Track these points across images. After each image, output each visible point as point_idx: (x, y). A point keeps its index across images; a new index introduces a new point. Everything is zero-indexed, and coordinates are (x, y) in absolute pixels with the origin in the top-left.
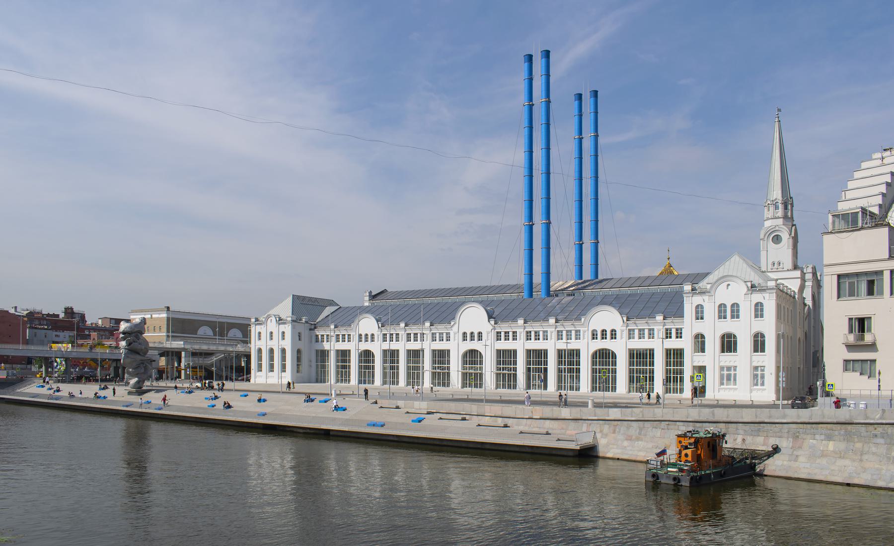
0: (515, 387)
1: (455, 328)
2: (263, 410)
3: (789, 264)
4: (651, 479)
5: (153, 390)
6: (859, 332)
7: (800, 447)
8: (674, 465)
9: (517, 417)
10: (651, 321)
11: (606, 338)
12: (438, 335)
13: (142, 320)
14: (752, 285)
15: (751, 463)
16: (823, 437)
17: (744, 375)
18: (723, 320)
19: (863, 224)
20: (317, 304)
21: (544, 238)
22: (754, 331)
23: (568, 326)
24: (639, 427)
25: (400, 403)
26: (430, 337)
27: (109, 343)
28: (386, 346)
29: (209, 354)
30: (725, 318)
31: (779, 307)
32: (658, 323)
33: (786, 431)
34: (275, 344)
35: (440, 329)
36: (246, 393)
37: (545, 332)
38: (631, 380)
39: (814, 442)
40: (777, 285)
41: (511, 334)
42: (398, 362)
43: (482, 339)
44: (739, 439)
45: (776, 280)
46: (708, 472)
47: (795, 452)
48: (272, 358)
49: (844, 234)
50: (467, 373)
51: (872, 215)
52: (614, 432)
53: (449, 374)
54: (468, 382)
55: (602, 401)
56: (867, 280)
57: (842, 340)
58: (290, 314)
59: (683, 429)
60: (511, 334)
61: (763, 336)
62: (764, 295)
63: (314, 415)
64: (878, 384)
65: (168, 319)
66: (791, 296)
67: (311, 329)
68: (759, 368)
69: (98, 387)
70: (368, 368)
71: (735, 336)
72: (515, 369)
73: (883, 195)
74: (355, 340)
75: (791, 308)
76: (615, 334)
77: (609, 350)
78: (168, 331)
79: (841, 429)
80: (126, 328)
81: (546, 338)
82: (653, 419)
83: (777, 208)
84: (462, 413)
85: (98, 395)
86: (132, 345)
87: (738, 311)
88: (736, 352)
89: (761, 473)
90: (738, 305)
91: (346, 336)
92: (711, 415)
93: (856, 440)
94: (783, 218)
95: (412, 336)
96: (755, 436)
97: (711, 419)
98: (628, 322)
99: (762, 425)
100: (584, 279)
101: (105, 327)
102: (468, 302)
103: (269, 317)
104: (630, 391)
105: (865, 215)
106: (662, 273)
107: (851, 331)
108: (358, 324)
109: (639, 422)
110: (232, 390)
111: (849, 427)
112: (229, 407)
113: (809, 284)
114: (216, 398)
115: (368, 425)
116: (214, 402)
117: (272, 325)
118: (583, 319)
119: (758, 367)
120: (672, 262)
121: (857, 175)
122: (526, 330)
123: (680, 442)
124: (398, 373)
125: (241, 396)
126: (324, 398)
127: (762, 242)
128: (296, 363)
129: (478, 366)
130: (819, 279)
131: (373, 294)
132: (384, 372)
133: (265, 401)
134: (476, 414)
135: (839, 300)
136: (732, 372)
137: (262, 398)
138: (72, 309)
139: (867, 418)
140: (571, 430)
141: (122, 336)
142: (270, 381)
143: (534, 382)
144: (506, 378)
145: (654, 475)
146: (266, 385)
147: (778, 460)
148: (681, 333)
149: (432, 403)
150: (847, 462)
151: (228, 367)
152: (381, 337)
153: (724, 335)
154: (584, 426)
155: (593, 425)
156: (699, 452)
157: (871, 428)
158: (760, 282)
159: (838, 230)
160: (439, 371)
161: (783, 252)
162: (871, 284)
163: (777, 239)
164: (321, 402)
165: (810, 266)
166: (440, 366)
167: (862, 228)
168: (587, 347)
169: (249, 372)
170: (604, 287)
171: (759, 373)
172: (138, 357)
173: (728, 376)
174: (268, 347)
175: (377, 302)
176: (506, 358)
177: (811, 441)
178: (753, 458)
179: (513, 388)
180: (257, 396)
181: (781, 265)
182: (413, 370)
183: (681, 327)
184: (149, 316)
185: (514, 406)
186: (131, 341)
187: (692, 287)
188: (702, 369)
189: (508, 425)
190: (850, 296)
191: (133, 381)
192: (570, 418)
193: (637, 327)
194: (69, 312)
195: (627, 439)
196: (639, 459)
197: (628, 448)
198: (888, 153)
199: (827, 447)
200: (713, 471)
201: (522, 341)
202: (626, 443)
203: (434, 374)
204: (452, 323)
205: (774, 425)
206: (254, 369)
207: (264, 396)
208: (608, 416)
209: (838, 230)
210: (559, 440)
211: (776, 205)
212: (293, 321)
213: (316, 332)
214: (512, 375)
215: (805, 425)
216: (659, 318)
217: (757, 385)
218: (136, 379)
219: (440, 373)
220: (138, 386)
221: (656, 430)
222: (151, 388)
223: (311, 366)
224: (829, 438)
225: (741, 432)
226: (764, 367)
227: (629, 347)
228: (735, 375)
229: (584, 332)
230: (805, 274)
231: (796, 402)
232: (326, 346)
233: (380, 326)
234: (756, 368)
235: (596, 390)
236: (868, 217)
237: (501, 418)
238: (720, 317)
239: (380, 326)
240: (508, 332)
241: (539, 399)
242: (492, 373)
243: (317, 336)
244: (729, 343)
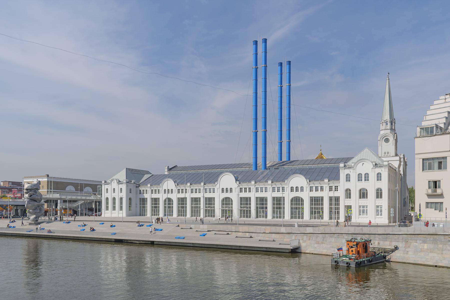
0: (250, 217)
1: (218, 186)
2: (115, 232)
3: (393, 153)
4: (334, 264)
5: (45, 222)
6: (434, 188)
7: (409, 247)
8: (346, 256)
9: (257, 232)
10: (322, 182)
11: (293, 191)
13: (38, 182)
14: (375, 164)
15: (384, 256)
16: (421, 242)
17: (371, 210)
18: (348, 182)
19: (436, 133)
20: (141, 173)
21: (263, 139)
22: (376, 187)
23: (278, 185)
24: (323, 237)
25: (192, 226)
27: (8, 196)
29: (75, 201)
31: (389, 175)
32: (326, 183)
34: (117, 195)
35: (208, 186)
36: (103, 222)
38: (311, 213)
39: (417, 244)
40: (389, 164)
41: (248, 189)
42: (172, 204)
44: (376, 243)
45: (388, 161)
46: (364, 260)
48: (114, 203)
49: (426, 138)
50: (224, 210)
51: (441, 128)
52: (309, 240)
53: (214, 210)
54: (225, 214)
55: (302, 224)
56: (439, 162)
57: (426, 192)
58: (125, 178)
59: (350, 238)
60: (248, 189)
61: (381, 190)
62: (382, 169)
63: (144, 233)
64: (446, 215)
65: (48, 181)
66: (393, 168)
67: (136, 187)
68: (379, 207)
69: (9, 221)
70: (155, 207)
71: (366, 190)
72: (250, 208)
73: (446, 118)
74: (162, 192)
75: (394, 176)
77: (300, 197)
78: (48, 189)
79: (431, 237)
80: (28, 187)
81: (250, 191)
82: (330, 233)
83: (387, 124)
84: (226, 231)
85: (9, 226)
86: (32, 196)
87: (368, 177)
88: (367, 198)
89: (389, 260)
90: (368, 174)
91: (157, 190)
93: (439, 243)
94: (390, 129)
96: (385, 241)
97: (361, 233)
98: (310, 183)
100: (283, 160)
101: (5, 187)
102: (225, 172)
103: (112, 180)
104: (311, 219)
105: (437, 128)
106: (317, 158)
107: (429, 188)
109: (323, 234)
110: (122, 222)
111: (435, 236)
112: (93, 230)
113: (402, 163)
114: (85, 225)
115: (176, 238)
116: (84, 228)
117: (115, 185)
118: (286, 181)
119: (379, 206)
120: (322, 152)
121: (432, 107)
122: (256, 187)
123: (348, 244)
124: (186, 210)
125: (100, 224)
126: (149, 224)
127: (379, 142)
128: (128, 206)
129: (230, 206)
130: (406, 161)
131: (170, 168)
132: (178, 210)
133: (114, 226)
134: (234, 231)
135: (423, 171)
136: (365, 209)
137: (113, 225)
139: (445, 232)
142: (120, 215)
143: (260, 214)
144: (245, 213)
145: (336, 262)
146: (111, 218)
147: (398, 253)
148: (337, 189)
149: (210, 225)
150: (435, 255)
151: (86, 209)
152: (177, 191)
153: (361, 190)
154: (293, 237)
155: (298, 236)
156: (358, 249)
157: (447, 237)
158: (379, 162)
159: (423, 136)
160: (209, 209)
161: (390, 147)
162: (440, 163)
163: (387, 140)
164: (147, 226)
165: (402, 155)
166: (210, 206)
167: (436, 135)
168: (288, 196)
169: (100, 210)
170: (325, 163)
171: (379, 209)
172: (36, 203)
173: (363, 211)
174: (106, 197)
175: (172, 172)
176: (245, 201)
177: (415, 243)
178: (385, 252)
179: (249, 218)
180: (110, 224)
181: (389, 153)
182: (194, 208)
183: (337, 185)
185: (255, 227)
186: (32, 194)
187: (344, 164)
188: (349, 208)
189: (252, 237)
190: (429, 170)
191: (33, 217)
192: (286, 232)
193: (276, 186)
195: (316, 243)
196: (323, 253)
197: (317, 248)
198: (448, 96)
199: (424, 247)
200: (366, 259)
201: (254, 192)
202: (316, 245)
204: (216, 183)
205: (395, 236)
206: (104, 209)
207: (114, 224)
208: (306, 231)
209: (423, 136)
210: (280, 244)
211: (386, 123)
212: (127, 182)
213: (140, 188)
214: (246, 211)
215: (411, 235)
216: (326, 181)
217: (378, 215)
218: (34, 216)
220: (36, 220)
222: (44, 221)
223: (137, 207)
224: (424, 242)
225: (377, 239)
226: (382, 206)
227: (273, 196)
228: (367, 210)
229: (287, 188)
230: (401, 158)
231: (401, 224)
232: (146, 196)
233: (176, 185)
234: (378, 206)
235: (293, 218)
236: (439, 129)
238: (347, 181)
239: (176, 185)
240: (246, 188)
241: (265, 223)
243: (140, 190)
244: (364, 193)
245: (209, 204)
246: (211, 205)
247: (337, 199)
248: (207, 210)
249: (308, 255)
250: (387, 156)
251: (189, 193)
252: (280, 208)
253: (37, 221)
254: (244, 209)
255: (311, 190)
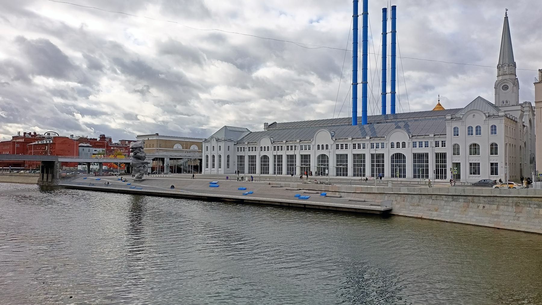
1: (313, 143)
11: (399, 147)
12: (304, 147)
18: (456, 136)
22: (491, 142)
26: (299, 147)
28: (275, 153)
30: (472, 134)
33: (511, 202)
37: (364, 144)
41: (344, 146)
42: (282, 162)
43: (365, 147)
47: (517, 215)
52: (404, 201)
67: (235, 145)
70: (241, 165)
76: (405, 145)
92: (463, 191)
95: (290, 147)
96: (491, 204)
99: (495, 198)
108: (260, 142)
124: (282, 168)
134: (324, 190)
138: (104, 135)
140: (378, 200)
141: (131, 150)
142: (213, 173)
144: (342, 171)
148: (445, 144)
152: (411, 144)
168: (388, 153)
174: (206, 155)
184: (147, 139)
188: (458, 165)
194: (103, 137)
202: (411, 208)
203: (301, 168)
219: (305, 167)
221: (430, 200)
223: (235, 165)
229: (386, 144)
237: (338, 193)
238: (469, 134)
239: (272, 142)
242: (334, 167)
245: (305, 162)
246: (343, 163)
247: (444, 155)
248: (302, 167)
249: (402, 217)
250: (502, 106)
251: (351, 149)
252: (293, 165)
253: (141, 178)
254: (341, 166)
255: (414, 146)
